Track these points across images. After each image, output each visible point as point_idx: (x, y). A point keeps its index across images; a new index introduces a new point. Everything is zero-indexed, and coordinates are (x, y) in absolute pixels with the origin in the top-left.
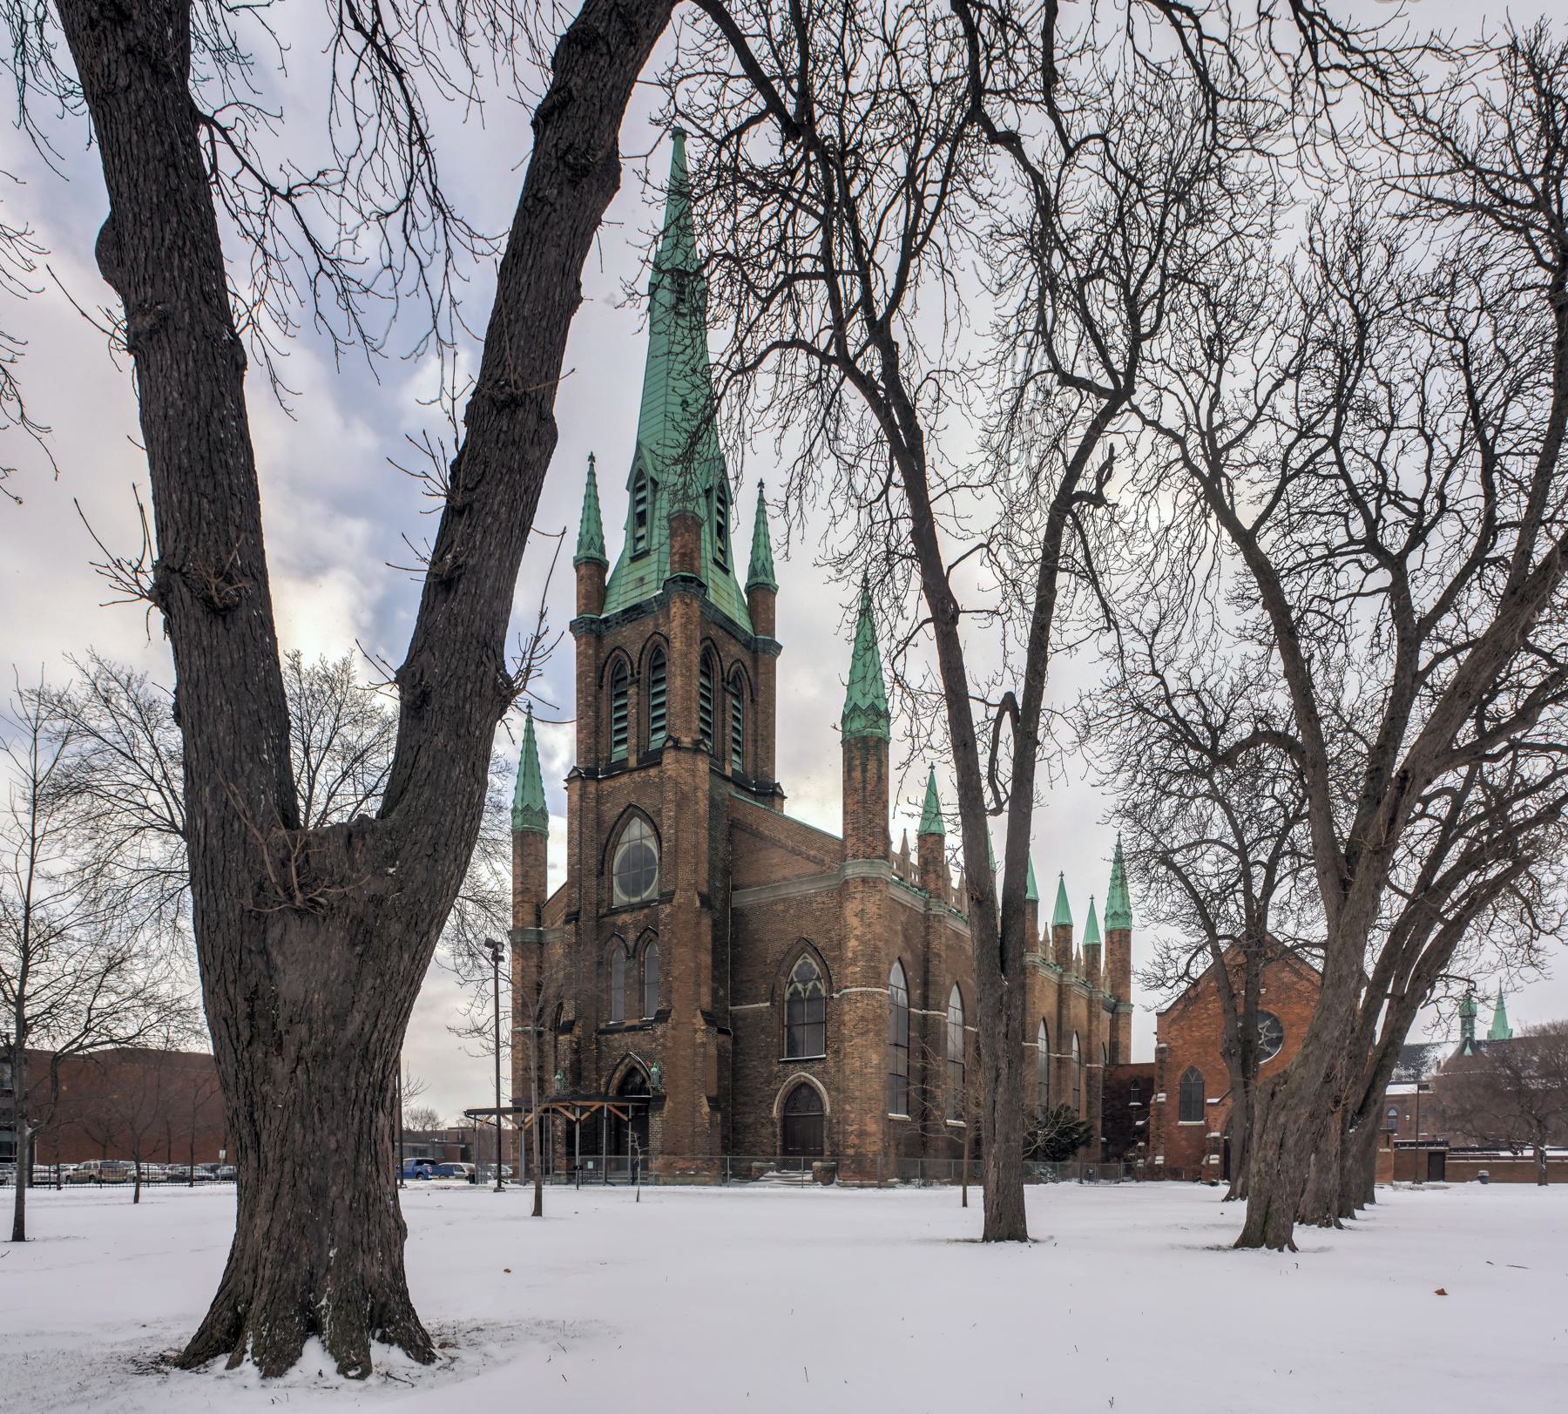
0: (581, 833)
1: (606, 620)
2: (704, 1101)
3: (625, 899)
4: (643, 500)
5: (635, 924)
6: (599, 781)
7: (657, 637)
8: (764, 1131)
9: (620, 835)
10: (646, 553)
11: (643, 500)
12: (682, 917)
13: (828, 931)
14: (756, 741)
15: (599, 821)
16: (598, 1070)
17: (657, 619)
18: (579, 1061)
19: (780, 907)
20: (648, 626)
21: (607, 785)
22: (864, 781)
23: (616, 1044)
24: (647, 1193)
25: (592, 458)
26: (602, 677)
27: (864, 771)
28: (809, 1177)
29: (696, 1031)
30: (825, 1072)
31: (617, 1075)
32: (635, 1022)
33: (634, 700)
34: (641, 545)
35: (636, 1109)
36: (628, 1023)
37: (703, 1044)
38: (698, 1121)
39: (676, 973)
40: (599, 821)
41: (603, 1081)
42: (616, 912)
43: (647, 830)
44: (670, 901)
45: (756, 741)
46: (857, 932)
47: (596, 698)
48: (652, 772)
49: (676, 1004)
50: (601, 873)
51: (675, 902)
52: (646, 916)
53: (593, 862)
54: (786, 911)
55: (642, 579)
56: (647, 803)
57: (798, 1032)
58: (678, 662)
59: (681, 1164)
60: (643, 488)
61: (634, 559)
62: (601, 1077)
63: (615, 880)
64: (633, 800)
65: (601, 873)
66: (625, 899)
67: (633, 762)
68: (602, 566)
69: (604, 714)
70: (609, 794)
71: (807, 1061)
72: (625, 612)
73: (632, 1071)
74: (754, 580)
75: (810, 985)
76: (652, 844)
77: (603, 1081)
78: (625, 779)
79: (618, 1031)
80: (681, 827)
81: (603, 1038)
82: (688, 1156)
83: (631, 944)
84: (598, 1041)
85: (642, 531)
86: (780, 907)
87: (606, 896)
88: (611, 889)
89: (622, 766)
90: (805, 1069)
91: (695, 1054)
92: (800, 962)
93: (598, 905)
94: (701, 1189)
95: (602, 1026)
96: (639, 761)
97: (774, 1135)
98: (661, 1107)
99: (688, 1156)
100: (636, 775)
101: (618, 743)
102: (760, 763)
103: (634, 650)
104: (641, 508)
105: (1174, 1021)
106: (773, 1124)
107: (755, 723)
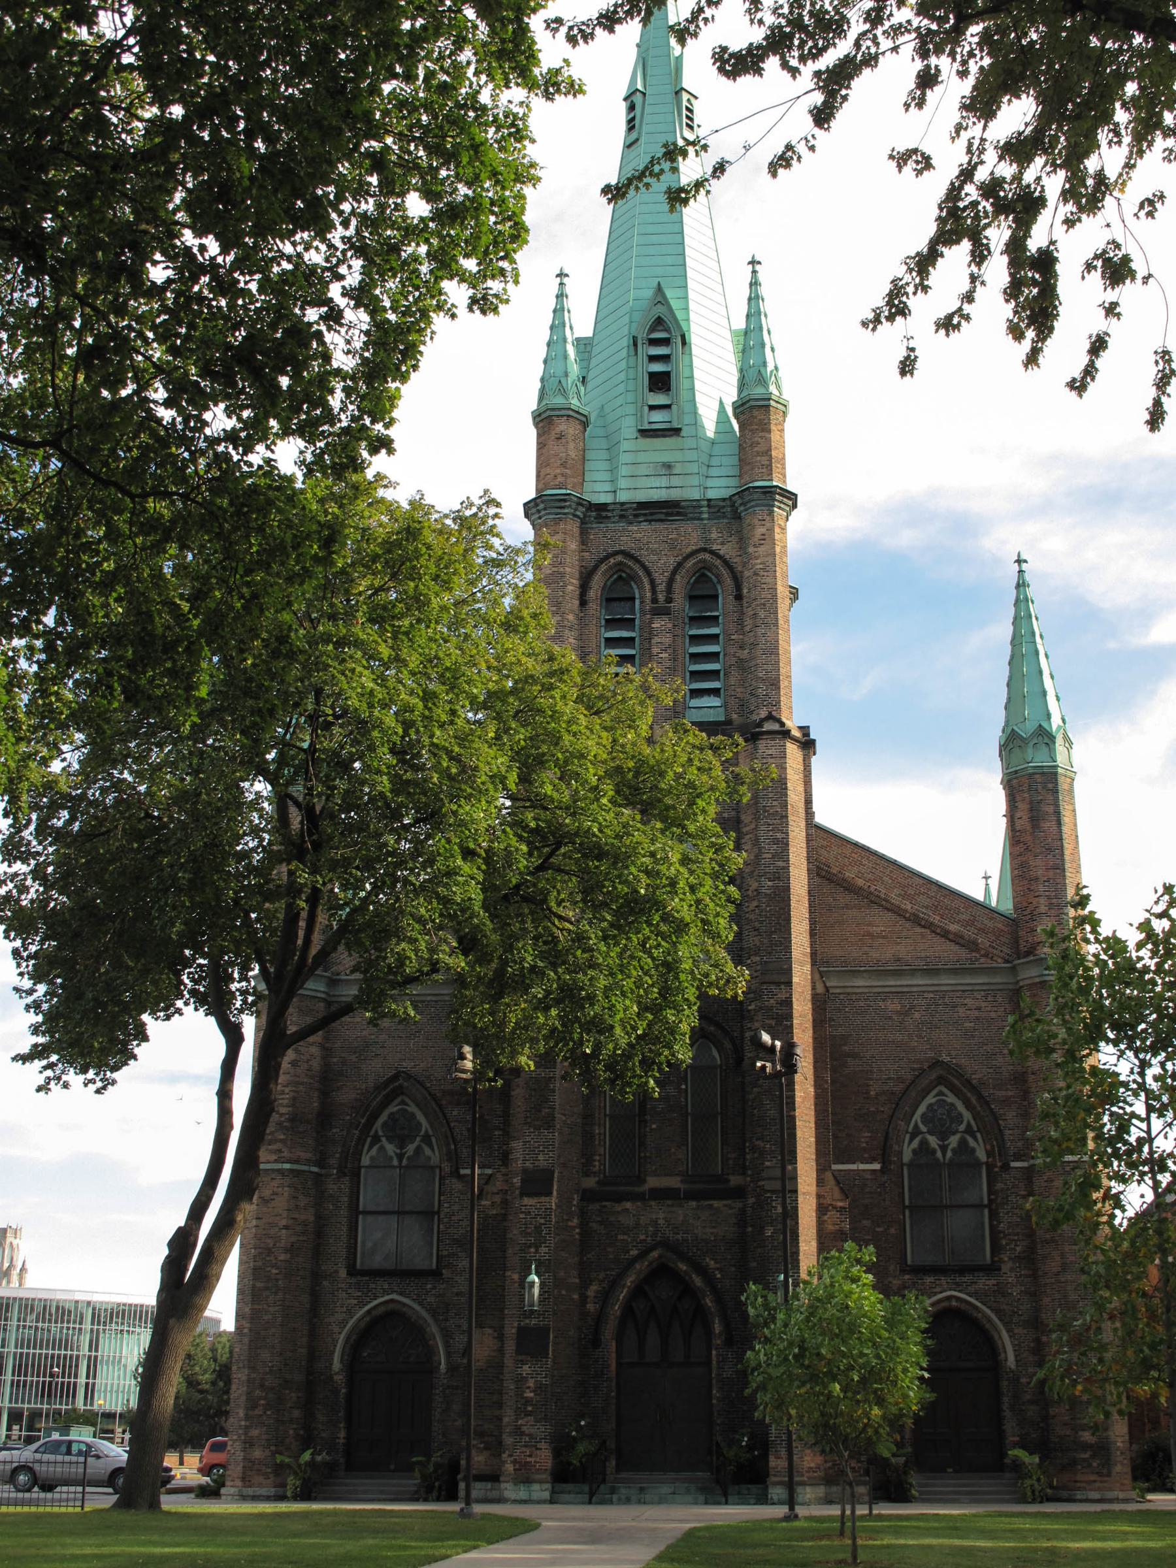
7: (707, 556)
33: (667, 639)
36: (653, 1182)
54: (905, 1013)
55: (668, 466)
62: (585, 1284)
72: (642, 505)
75: (954, 1141)
81: (594, 1207)
86: (893, 1005)
90: (957, 1286)
92: (930, 1099)
103: (661, 563)
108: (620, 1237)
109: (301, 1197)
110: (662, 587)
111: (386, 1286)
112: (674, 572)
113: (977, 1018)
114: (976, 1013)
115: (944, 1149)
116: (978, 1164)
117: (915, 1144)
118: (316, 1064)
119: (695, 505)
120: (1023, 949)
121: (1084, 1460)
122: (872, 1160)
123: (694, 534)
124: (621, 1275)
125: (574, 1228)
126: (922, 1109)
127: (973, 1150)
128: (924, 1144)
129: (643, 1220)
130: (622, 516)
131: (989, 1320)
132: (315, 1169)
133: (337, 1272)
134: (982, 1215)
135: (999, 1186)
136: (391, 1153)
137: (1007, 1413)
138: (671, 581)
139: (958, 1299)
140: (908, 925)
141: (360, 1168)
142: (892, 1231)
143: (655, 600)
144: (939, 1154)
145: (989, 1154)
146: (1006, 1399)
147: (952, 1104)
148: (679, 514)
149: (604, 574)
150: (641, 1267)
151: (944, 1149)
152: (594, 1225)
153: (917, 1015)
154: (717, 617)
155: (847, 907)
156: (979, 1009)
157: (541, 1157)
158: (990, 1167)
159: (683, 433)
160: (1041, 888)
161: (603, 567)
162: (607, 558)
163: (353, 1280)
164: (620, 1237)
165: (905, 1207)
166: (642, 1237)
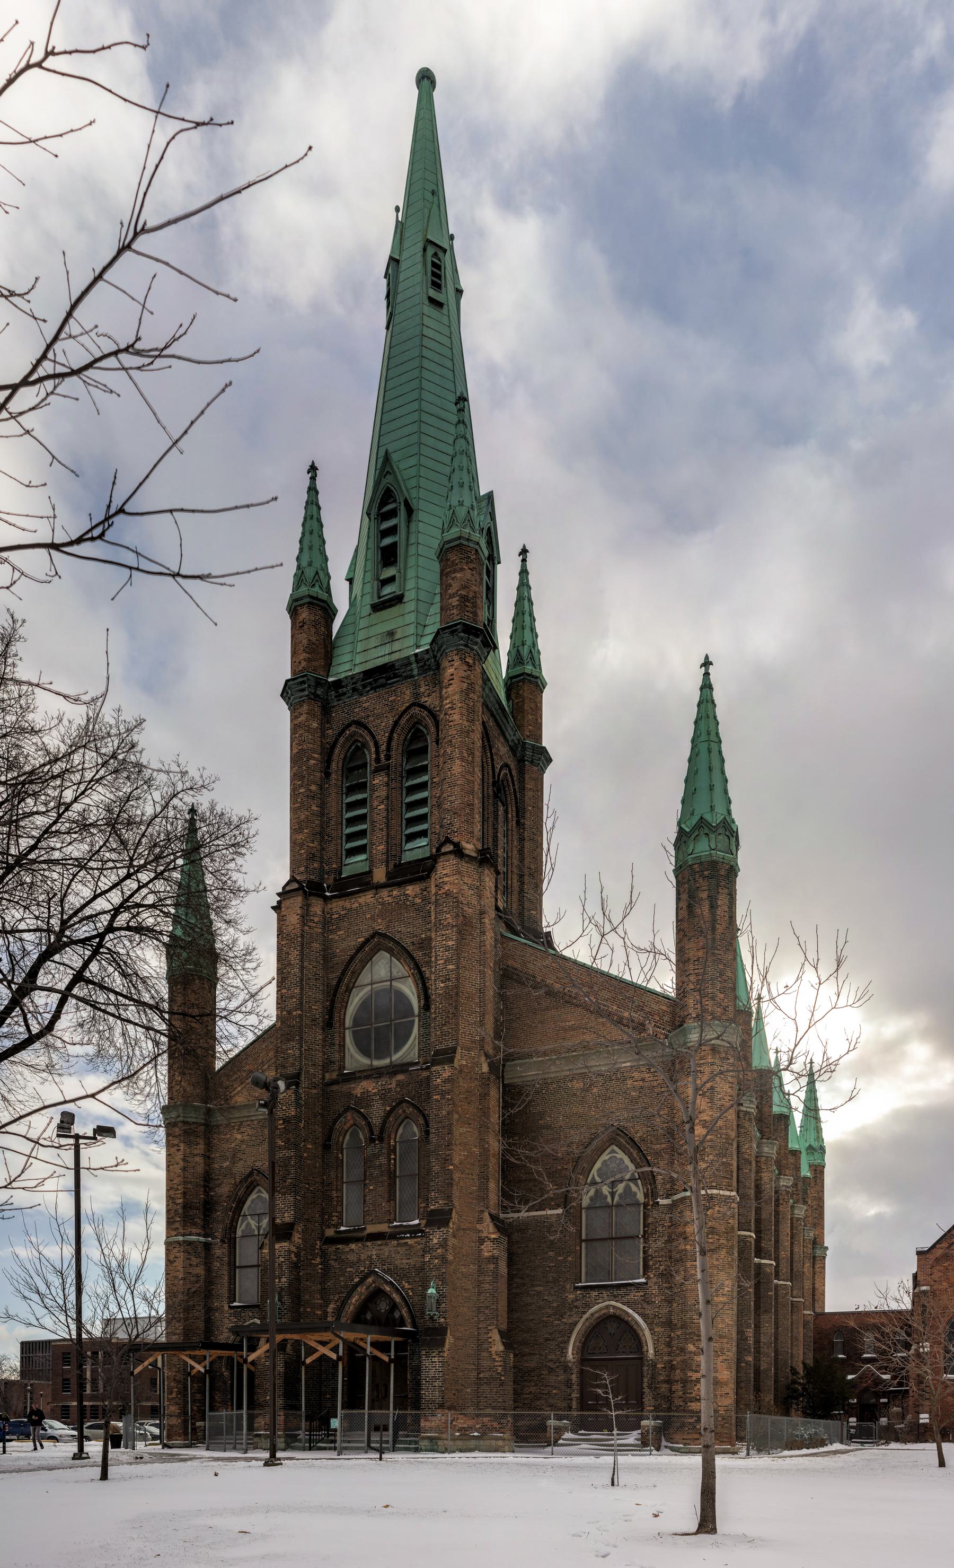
0: (302, 968)
1: (338, 684)
2: (496, 1336)
3: (365, 1061)
4: (393, 531)
5: (384, 1095)
6: (326, 899)
7: (416, 710)
8: (552, 1379)
9: (356, 974)
10: (398, 599)
11: (393, 531)
12: (463, 1084)
13: (650, 1117)
14: (521, 876)
15: (327, 957)
16: (324, 1293)
17: (416, 686)
18: (298, 1279)
19: (578, 1085)
20: (405, 695)
21: (338, 906)
22: (714, 921)
23: (352, 1257)
24: (635, 1468)
25: (313, 469)
26: (329, 761)
27: (713, 907)
28: (632, 1438)
29: (481, 1241)
30: (647, 1300)
31: (354, 1300)
32: (383, 1228)
33: (383, 792)
34: (388, 590)
35: (400, 1347)
36: (371, 1229)
37: (494, 1259)
38: (485, 1363)
39: (456, 1160)
40: (327, 957)
41: (331, 1308)
42: (353, 1077)
43: (400, 968)
44: (451, 1061)
45: (521, 876)
46: (704, 1117)
47: (321, 787)
48: (411, 890)
49: (456, 1202)
50: (329, 1024)
51: (456, 1064)
52: (399, 1084)
53: (317, 1009)
54: (587, 1090)
55: (391, 633)
56: (404, 931)
57: (46, 1311)
58: (457, 740)
59: (462, 1422)
60: (393, 514)
61: (377, 607)
62: (327, 1303)
63: (348, 1034)
64: (380, 926)
65: (329, 1024)
66: (365, 1061)
67: (380, 875)
68: (329, 611)
69: (333, 810)
70: (342, 918)
71: (619, 1287)
72: (368, 674)
73: (377, 1294)
74: (518, 670)
75: (620, 1188)
76: (409, 990)
77: (331, 1308)
78: (367, 898)
79: (358, 1240)
80: (463, 962)
81: (332, 1249)
82: (471, 1411)
83: (376, 1120)
84: (324, 1254)
85: (389, 572)
86: (578, 1085)
87: (336, 1056)
88: (342, 1046)
89: (363, 882)
90: (615, 1298)
91: (481, 1272)
92: (605, 1157)
93: (326, 1067)
94: (495, 1457)
95: (330, 1232)
96: (389, 875)
97: (568, 1384)
98: (442, 1344)
99: (471, 1411)
100: (384, 893)
101: (352, 852)
102: (527, 905)
103: (382, 726)
104: (387, 541)
105: (937, 1260)
106: (566, 1369)
107: (521, 852)
108: (348, 1270)
109: (193, 1258)
110: (383, 747)
111: (251, 1314)
112: (392, 732)
113: (642, 1088)
114: (641, 1083)
115: (613, 1194)
116: (637, 1204)
117: (592, 1193)
118: (200, 1169)
119: (406, 662)
120: (677, 1024)
121: (690, 1423)
122: (557, 1206)
123: (408, 692)
124: (349, 1296)
125: (318, 1264)
126: (598, 1165)
127: (635, 1194)
128: (598, 1193)
129: (363, 1257)
130: (354, 690)
131: (637, 1323)
132: (202, 1239)
133: (223, 1306)
134: (587, 1234)
135: (650, 1220)
136: (254, 1227)
137: (646, 1390)
138: (390, 739)
139: (614, 1307)
140: (593, 1017)
141: (235, 1238)
142: (570, 1259)
143: (378, 760)
144: (609, 1200)
145: (646, 1195)
146: (645, 1380)
147: (621, 1159)
148: (396, 676)
149: (343, 746)
150: (362, 1289)
151: (613, 1194)
152: (332, 1262)
153: (595, 1090)
154: (427, 765)
155: (547, 1009)
156: (643, 1080)
157: (286, 1215)
158: (645, 1205)
159: (405, 600)
160: (691, 967)
161: (342, 740)
162: (343, 731)
163: (232, 1311)
164: (348, 1270)
165: (582, 1241)
166: (362, 1269)
